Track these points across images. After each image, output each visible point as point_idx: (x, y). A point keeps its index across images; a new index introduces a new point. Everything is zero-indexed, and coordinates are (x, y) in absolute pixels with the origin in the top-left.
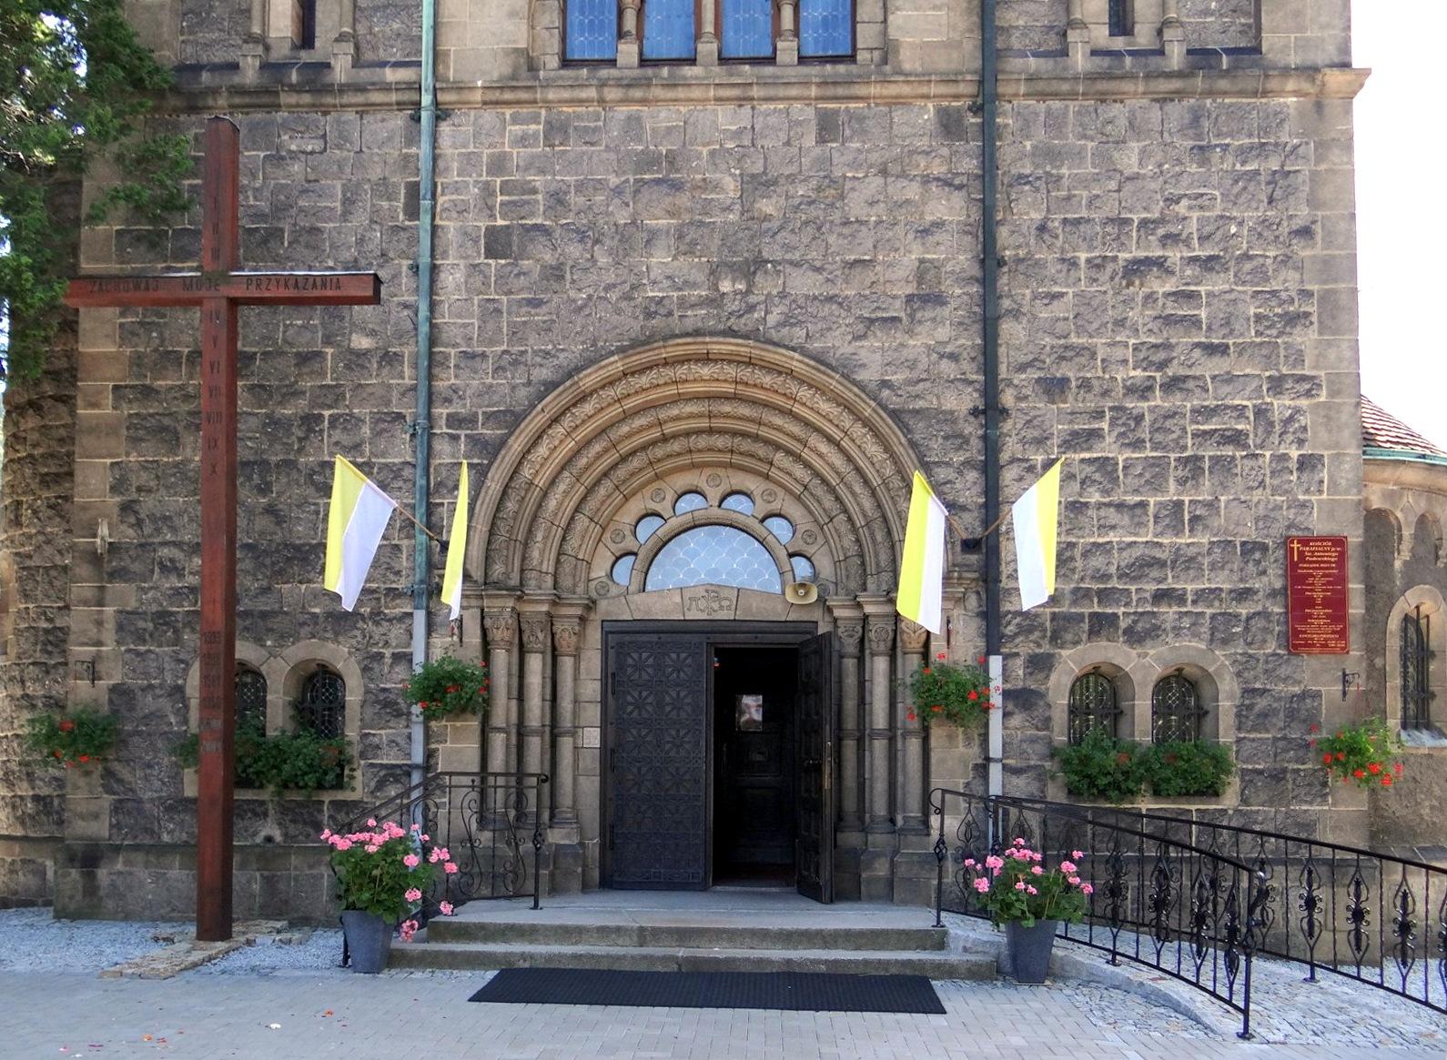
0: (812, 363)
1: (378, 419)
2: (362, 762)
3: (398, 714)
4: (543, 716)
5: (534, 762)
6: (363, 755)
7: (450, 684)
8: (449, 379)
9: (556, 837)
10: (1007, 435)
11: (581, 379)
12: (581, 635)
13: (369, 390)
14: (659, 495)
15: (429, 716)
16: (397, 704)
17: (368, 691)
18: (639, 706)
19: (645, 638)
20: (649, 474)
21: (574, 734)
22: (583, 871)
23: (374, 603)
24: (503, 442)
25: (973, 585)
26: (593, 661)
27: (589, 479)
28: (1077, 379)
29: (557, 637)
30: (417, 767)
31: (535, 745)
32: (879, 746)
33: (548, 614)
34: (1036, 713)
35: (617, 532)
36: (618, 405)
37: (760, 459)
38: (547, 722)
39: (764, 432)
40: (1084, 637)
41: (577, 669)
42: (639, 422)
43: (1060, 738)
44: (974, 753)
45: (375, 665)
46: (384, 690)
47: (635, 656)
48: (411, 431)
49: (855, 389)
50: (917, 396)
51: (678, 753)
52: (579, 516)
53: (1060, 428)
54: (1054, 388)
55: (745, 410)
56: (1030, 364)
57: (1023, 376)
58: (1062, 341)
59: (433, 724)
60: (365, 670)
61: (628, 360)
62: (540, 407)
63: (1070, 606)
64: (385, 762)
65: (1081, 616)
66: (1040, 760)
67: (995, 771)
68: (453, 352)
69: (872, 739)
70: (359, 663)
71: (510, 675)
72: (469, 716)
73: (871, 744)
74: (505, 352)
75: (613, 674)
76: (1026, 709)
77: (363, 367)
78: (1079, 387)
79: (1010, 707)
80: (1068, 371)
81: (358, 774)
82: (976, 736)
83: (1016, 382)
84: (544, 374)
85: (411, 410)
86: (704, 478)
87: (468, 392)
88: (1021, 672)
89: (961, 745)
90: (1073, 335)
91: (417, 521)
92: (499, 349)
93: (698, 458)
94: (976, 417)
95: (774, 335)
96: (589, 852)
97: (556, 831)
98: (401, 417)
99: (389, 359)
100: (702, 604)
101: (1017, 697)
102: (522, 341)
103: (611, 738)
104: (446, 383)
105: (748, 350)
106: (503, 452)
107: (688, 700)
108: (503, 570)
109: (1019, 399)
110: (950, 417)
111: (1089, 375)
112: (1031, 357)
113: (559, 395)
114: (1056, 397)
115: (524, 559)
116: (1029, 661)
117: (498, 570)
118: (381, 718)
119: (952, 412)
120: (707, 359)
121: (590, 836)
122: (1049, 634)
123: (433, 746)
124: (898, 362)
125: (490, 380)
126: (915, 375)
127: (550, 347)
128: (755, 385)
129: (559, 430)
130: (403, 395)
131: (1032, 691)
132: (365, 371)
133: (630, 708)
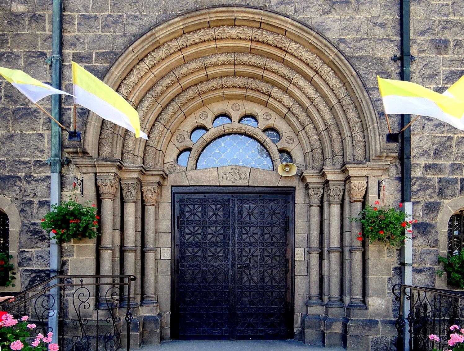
0: (299, 25)
1: (29, 56)
2: (20, 269)
3: (43, 239)
4: (136, 240)
5: (131, 268)
6: (20, 264)
7: (72, 218)
8: (74, 32)
9: (144, 311)
10: (413, 73)
11: (157, 32)
12: (159, 194)
13: (23, 37)
14: (204, 115)
15: (61, 241)
16: (41, 232)
17: (23, 225)
18: (194, 235)
19: (196, 196)
20: (198, 101)
21: (155, 251)
22: (161, 332)
23: (27, 170)
24: (108, 70)
25: (394, 161)
26: (166, 210)
27: (164, 100)
28: (454, 41)
29: (145, 194)
30: (54, 271)
31: (131, 259)
32: (335, 257)
33: (138, 179)
34: (430, 237)
35: (180, 136)
36: (180, 53)
37: (263, 93)
38: (139, 243)
39: (267, 74)
40: (458, 192)
41: (157, 213)
42: (193, 65)
43: (444, 252)
44: (394, 261)
45: (27, 208)
46: (34, 224)
47: (191, 206)
48: (49, 63)
49: (325, 42)
50: (361, 48)
51: (215, 262)
52: (157, 124)
53: (444, 70)
54: (440, 46)
55: (256, 60)
56: (427, 31)
57: (423, 38)
58: (445, 18)
59: (65, 245)
60: (22, 211)
61: (185, 22)
62: (131, 48)
63: (449, 174)
64: (34, 268)
65: (456, 179)
66: (432, 264)
67: (408, 272)
68: (76, 15)
69: (329, 253)
70: (18, 207)
71: (114, 215)
72: (87, 239)
73: (329, 256)
74: (109, 16)
75: (178, 217)
76: (425, 235)
77: (19, 23)
78: (455, 45)
79: (416, 233)
80: (448, 36)
81: (18, 276)
82: (395, 251)
83: (418, 41)
84: (134, 29)
85: (51, 51)
86: (230, 106)
87: (86, 40)
88: (421, 213)
89: (386, 256)
90: (451, 14)
91: (53, 117)
92: (106, 14)
93: (227, 92)
94: (395, 61)
95: (275, 9)
96: (164, 320)
97: (144, 308)
98: (43, 54)
99: (36, 18)
100: (229, 177)
101: (419, 228)
102: (120, 9)
103: (177, 254)
104: (72, 34)
105: (259, 17)
106: (108, 76)
107: (222, 232)
108: (109, 151)
109: (421, 51)
110: (379, 62)
111: (460, 39)
112: (427, 27)
113: (146, 39)
114: (442, 50)
115: (123, 146)
116: (426, 207)
117: (106, 151)
118: (32, 241)
119: (381, 59)
120: (234, 23)
121: (164, 310)
122: (437, 191)
123: (65, 259)
124: (349, 28)
125: (100, 33)
126: (359, 36)
127: (137, 13)
128: (263, 43)
129: (144, 66)
130: (45, 41)
131: (427, 224)
132: (20, 26)
133: (188, 237)
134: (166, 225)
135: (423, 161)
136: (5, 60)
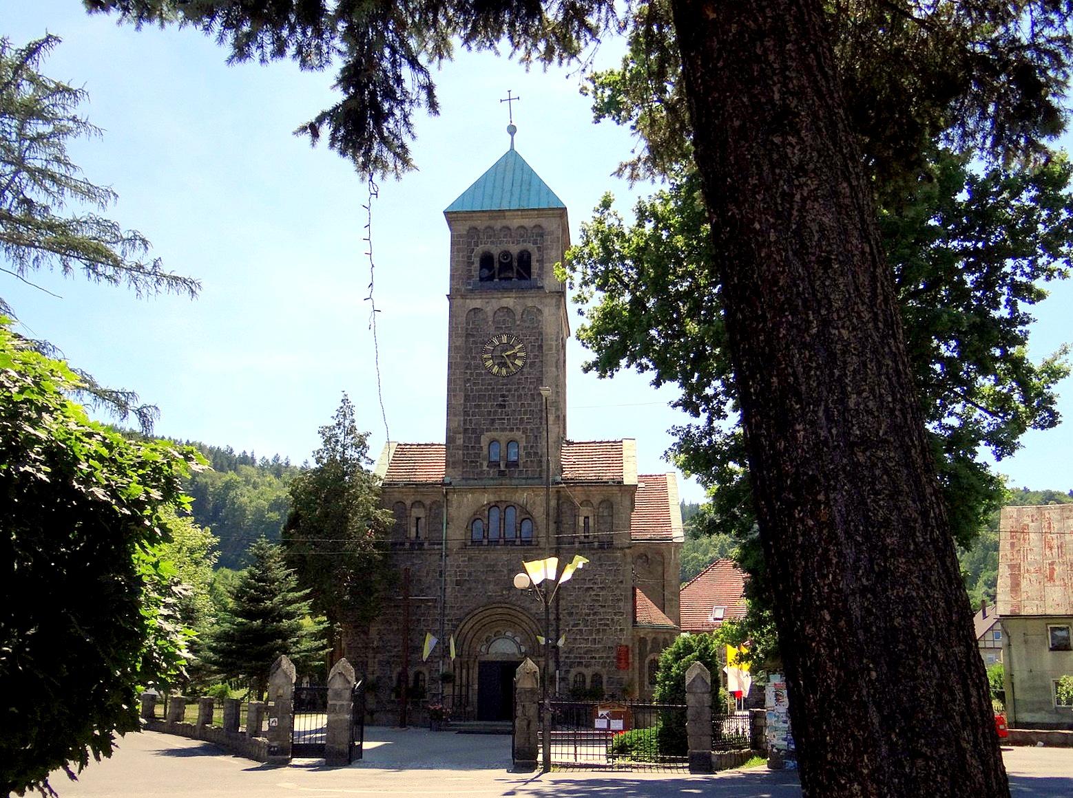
53: (572, 623)
80: (573, 610)
134: (476, 676)
135: (564, 655)
136: (450, 30)
